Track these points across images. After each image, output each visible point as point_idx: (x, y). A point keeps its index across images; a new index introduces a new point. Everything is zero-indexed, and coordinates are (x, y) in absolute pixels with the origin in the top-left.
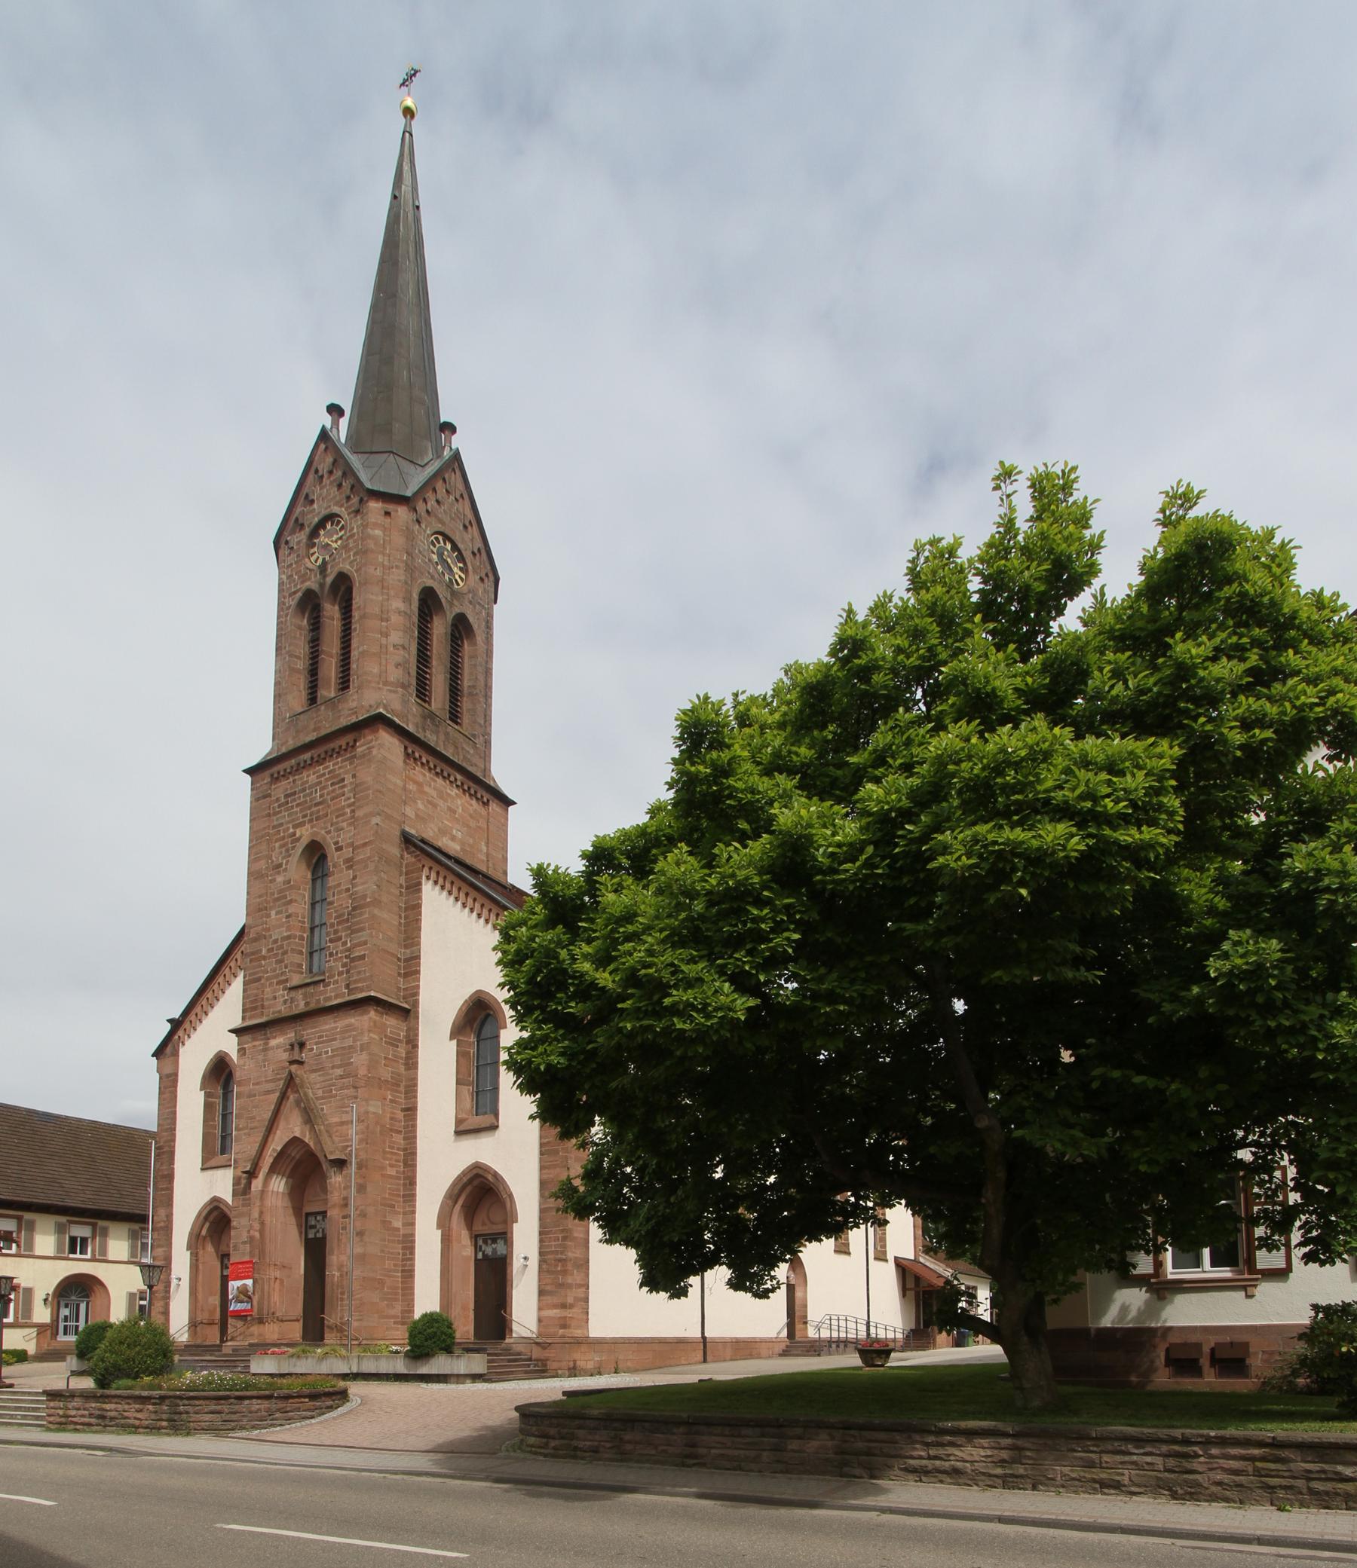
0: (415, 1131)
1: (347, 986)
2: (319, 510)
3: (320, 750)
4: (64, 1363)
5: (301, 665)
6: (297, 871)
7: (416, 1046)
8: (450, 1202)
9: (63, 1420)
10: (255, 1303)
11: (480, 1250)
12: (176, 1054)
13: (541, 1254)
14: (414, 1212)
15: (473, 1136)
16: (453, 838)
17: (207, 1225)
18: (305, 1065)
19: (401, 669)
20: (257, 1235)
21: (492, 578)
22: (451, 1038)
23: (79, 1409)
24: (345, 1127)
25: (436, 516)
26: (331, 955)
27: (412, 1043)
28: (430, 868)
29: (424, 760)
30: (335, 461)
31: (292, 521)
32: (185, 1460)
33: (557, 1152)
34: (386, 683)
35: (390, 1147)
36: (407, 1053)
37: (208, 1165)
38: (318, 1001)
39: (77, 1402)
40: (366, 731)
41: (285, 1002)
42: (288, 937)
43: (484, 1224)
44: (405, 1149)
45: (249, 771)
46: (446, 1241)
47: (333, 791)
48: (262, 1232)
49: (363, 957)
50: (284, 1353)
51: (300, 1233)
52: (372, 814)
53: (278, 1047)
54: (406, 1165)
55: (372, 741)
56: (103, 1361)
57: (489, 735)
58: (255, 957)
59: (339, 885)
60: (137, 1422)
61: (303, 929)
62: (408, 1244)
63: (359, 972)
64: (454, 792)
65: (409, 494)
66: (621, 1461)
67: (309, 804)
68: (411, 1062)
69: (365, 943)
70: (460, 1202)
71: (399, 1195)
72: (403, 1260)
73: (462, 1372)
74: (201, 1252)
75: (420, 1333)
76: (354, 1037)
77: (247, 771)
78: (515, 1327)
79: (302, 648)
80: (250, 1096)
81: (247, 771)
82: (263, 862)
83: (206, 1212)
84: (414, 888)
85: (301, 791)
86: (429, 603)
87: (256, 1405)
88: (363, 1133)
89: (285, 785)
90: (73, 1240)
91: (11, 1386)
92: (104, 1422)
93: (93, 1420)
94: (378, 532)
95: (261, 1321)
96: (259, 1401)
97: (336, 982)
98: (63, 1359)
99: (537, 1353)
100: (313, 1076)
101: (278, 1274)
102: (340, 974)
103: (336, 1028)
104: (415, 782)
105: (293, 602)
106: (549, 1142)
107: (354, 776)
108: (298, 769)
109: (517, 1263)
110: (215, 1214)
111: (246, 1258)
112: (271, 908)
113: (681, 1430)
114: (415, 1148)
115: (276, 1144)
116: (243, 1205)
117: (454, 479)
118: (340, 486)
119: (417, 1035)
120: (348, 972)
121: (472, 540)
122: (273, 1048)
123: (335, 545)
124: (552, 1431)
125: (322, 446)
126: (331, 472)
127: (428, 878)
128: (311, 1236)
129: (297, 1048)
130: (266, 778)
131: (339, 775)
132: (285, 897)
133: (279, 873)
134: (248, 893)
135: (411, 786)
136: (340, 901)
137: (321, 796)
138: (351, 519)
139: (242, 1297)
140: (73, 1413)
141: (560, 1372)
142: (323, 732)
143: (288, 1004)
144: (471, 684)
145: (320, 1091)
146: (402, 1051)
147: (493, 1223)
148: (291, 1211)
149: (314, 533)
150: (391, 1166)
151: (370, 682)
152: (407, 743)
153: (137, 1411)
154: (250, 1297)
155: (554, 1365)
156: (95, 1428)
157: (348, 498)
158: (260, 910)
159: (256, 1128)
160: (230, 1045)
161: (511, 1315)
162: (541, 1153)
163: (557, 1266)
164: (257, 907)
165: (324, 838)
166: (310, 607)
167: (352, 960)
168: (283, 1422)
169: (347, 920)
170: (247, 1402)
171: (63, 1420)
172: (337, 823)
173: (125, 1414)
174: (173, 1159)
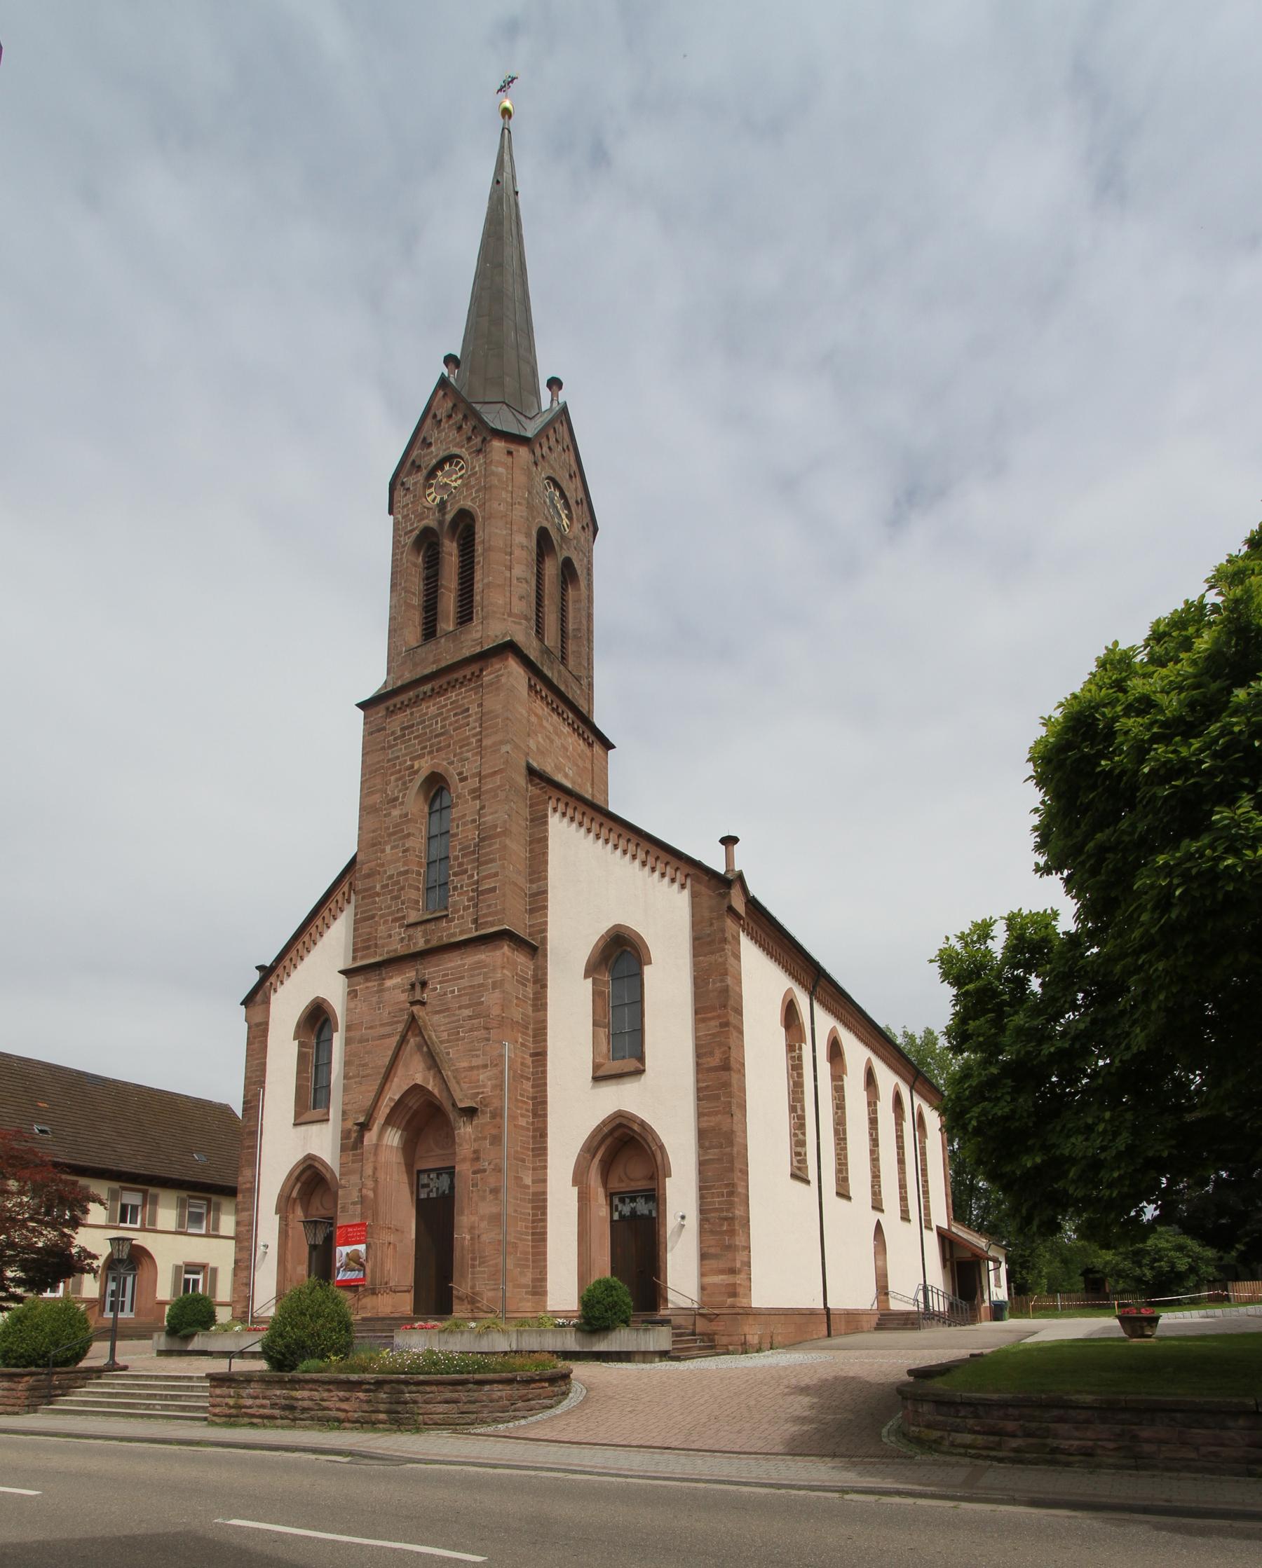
0: (545, 1078)
1: (475, 921)
2: (437, 452)
3: (443, 681)
4: (150, 1342)
5: (417, 601)
6: (414, 803)
7: (545, 986)
8: (588, 1156)
9: (233, 1411)
11: (617, 1210)
12: (267, 1002)
13: (702, 1211)
14: (545, 1167)
15: (614, 1081)
16: (566, 776)
17: (298, 1186)
18: (427, 1006)
19: (524, 602)
20: (371, 1194)
21: (591, 528)
22: (586, 977)
23: (256, 1398)
24: (475, 1072)
25: (549, 462)
26: (455, 888)
27: (540, 982)
28: (558, 800)
29: (544, 694)
30: (455, 405)
31: (408, 464)
32: (490, 1471)
33: (717, 1097)
34: (510, 614)
35: (522, 1095)
36: (534, 994)
37: (297, 1122)
38: (441, 938)
39: (254, 1389)
41: (402, 940)
42: (406, 872)
43: (621, 1180)
44: (534, 1098)
45: (362, 706)
47: (456, 722)
48: (375, 1190)
49: (493, 890)
50: (433, 1327)
51: (412, 1193)
52: (502, 742)
53: (395, 987)
54: (535, 1115)
55: (500, 669)
56: (281, 1336)
57: (592, 678)
58: (369, 894)
60: (341, 1415)
61: (420, 864)
62: (539, 1204)
63: (489, 906)
64: (566, 730)
65: (529, 434)
66: (1137, 1468)
67: (428, 735)
68: (540, 1002)
69: (496, 875)
70: (599, 1156)
71: (528, 1149)
72: (533, 1222)
73: (652, 1349)
74: (291, 1216)
75: (598, 1302)
76: (485, 974)
77: (360, 705)
78: (671, 1296)
79: (416, 584)
80: (361, 1041)
81: (360, 705)
82: (378, 795)
83: (298, 1171)
84: (539, 821)
85: (418, 724)
86: (544, 543)
87: (500, 1392)
89: (401, 718)
90: (124, 1207)
91: (125, 1368)
92: (292, 1414)
93: (277, 1412)
94: (501, 470)
95: (374, 1292)
96: (500, 1387)
97: (462, 917)
98: (150, 1338)
99: (701, 1325)
100: (436, 1017)
101: (392, 1238)
102: (466, 908)
103: (464, 965)
104: (536, 715)
105: (409, 540)
106: (707, 1087)
107: (481, 705)
108: (417, 701)
109: (671, 1222)
110: (308, 1173)
111: (357, 1221)
112: (386, 843)
113: (1241, 1422)
114: (546, 1096)
115: (394, 1092)
116: (353, 1162)
117: (562, 430)
118: (460, 428)
119: (546, 974)
120: (476, 906)
121: (576, 490)
122: (389, 989)
123: (454, 484)
124: (1011, 1426)
125: (441, 393)
126: (450, 417)
127: (555, 810)
128: (423, 1196)
129: (418, 988)
130: (381, 710)
131: (463, 705)
132: (402, 830)
133: (395, 807)
134: (360, 828)
135: (534, 719)
136: (465, 833)
137: (442, 727)
138: (472, 458)
140: (249, 1402)
141: (731, 1348)
142: (443, 664)
143: (406, 942)
144: (576, 627)
145: (446, 1033)
146: (530, 991)
147: (632, 1180)
148: (404, 1169)
149: (432, 474)
150: (522, 1116)
151: (494, 612)
152: (531, 675)
153: (341, 1400)
154: (362, 1265)
155: (724, 1340)
156: (279, 1422)
157: (469, 439)
158: (374, 845)
160: (335, 993)
161: (666, 1282)
162: (699, 1099)
163: (722, 1225)
164: (370, 839)
165: (447, 770)
166: (426, 545)
167: (479, 894)
168: (526, 1413)
169: (473, 852)
170: (487, 1387)
171: (233, 1411)
172: (462, 753)
173: (324, 1404)
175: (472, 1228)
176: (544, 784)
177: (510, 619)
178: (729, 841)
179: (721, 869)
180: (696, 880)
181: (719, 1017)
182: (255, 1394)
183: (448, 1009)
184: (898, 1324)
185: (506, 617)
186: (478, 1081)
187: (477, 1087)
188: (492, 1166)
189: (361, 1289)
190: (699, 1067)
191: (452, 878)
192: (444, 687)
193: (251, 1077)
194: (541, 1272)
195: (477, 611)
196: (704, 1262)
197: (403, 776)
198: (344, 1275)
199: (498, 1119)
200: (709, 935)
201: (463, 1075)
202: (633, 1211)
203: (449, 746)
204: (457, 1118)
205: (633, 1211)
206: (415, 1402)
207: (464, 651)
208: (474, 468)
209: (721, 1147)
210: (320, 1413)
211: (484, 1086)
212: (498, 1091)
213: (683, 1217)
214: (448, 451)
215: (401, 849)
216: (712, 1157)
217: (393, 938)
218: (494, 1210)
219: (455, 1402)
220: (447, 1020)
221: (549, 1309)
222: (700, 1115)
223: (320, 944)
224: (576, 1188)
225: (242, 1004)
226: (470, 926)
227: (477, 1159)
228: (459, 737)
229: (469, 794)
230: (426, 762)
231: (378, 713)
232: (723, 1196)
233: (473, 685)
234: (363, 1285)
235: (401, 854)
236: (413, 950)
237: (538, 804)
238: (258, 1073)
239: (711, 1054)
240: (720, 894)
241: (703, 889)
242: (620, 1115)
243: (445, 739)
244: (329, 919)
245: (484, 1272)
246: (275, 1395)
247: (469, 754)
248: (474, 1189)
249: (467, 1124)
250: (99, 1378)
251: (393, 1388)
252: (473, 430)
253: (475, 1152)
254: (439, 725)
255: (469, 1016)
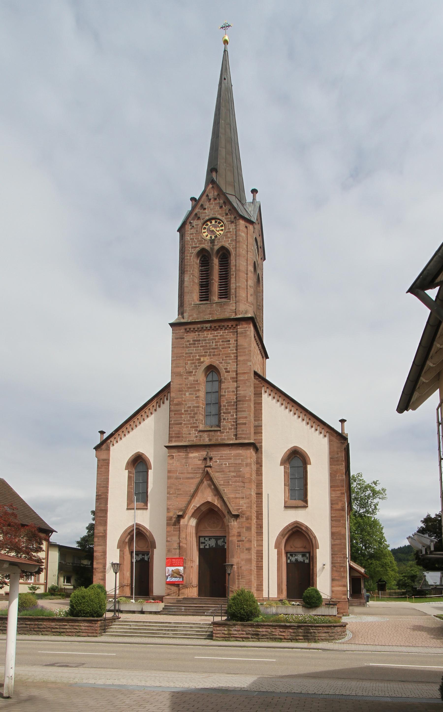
1: (236, 435)
3: (217, 325)
7: (261, 466)
9: (227, 636)
10: (184, 578)
11: (289, 559)
12: (108, 449)
13: (332, 563)
15: (294, 509)
18: (212, 468)
24: (238, 500)
26: (224, 419)
27: (259, 463)
33: (340, 521)
38: (217, 440)
40: (243, 323)
46: (279, 554)
49: (245, 424)
53: (194, 457)
55: (246, 328)
59: (228, 388)
63: (243, 430)
67: (208, 347)
80: (177, 478)
82: (181, 369)
84: (258, 395)
85: (202, 341)
88: (248, 504)
100: (217, 474)
103: (231, 454)
106: (335, 516)
108: (202, 330)
111: (177, 556)
112: (186, 391)
115: (197, 502)
116: (174, 531)
122: (191, 458)
127: (266, 392)
128: (202, 547)
129: (208, 460)
133: (191, 376)
137: (215, 345)
138: (228, 224)
139: (175, 575)
140: (235, 632)
143: (198, 438)
149: (205, 223)
153: (281, 632)
154: (181, 575)
159: (181, 494)
162: (332, 520)
165: (218, 365)
170: (336, 628)
171: (227, 636)
174: (107, 502)
175: (238, 563)
176: (260, 380)
177: (248, 304)
178: (342, 421)
179: (340, 432)
180: (331, 434)
181: (340, 490)
182: (238, 630)
183: (223, 471)
184: (358, 604)
185: (246, 303)
186: (240, 504)
187: (239, 506)
188: (247, 539)
189: (180, 586)
190: (332, 509)
191: (222, 414)
192: (217, 327)
193: (100, 484)
194: (261, 582)
195: (233, 297)
196: (333, 582)
197: (195, 363)
198: (171, 579)
199: (249, 520)
200: (337, 458)
201: (232, 500)
202: (296, 560)
203: (220, 355)
204: (230, 518)
205: (296, 560)
206: (315, 633)
207: (226, 313)
208: (230, 229)
209: (341, 539)
210: (271, 637)
211: (242, 506)
212: (249, 509)
213: (324, 565)
214: (215, 215)
215: (195, 396)
216: (337, 543)
217: (191, 435)
218: (248, 557)
219: (328, 633)
220: (223, 476)
221: (264, 596)
222: (332, 527)
223: (139, 427)
224: (276, 550)
225: (94, 449)
226: (233, 437)
227: (240, 536)
228: (224, 352)
229: (231, 379)
230: (208, 359)
231: (181, 330)
232: (341, 558)
233: (232, 331)
234: (182, 584)
235: (194, 398)
236: (202, 443)
237: (257, 388)
238: (105, 483)
239: (337, 504)
240: (341, 442)
241: (334, 439)
242: (296, 522)
243: (217, 351)
244: (145, 416)
245: (243, 582)
246: (249, 630)
247: (230, 361)
248: (238, 548)
249: (235, 521)
250: (115, 622)
251: (306, 628)
252: (229, 211)
253: (238, 533)
254: (214, 344)
255: (234, 476)
